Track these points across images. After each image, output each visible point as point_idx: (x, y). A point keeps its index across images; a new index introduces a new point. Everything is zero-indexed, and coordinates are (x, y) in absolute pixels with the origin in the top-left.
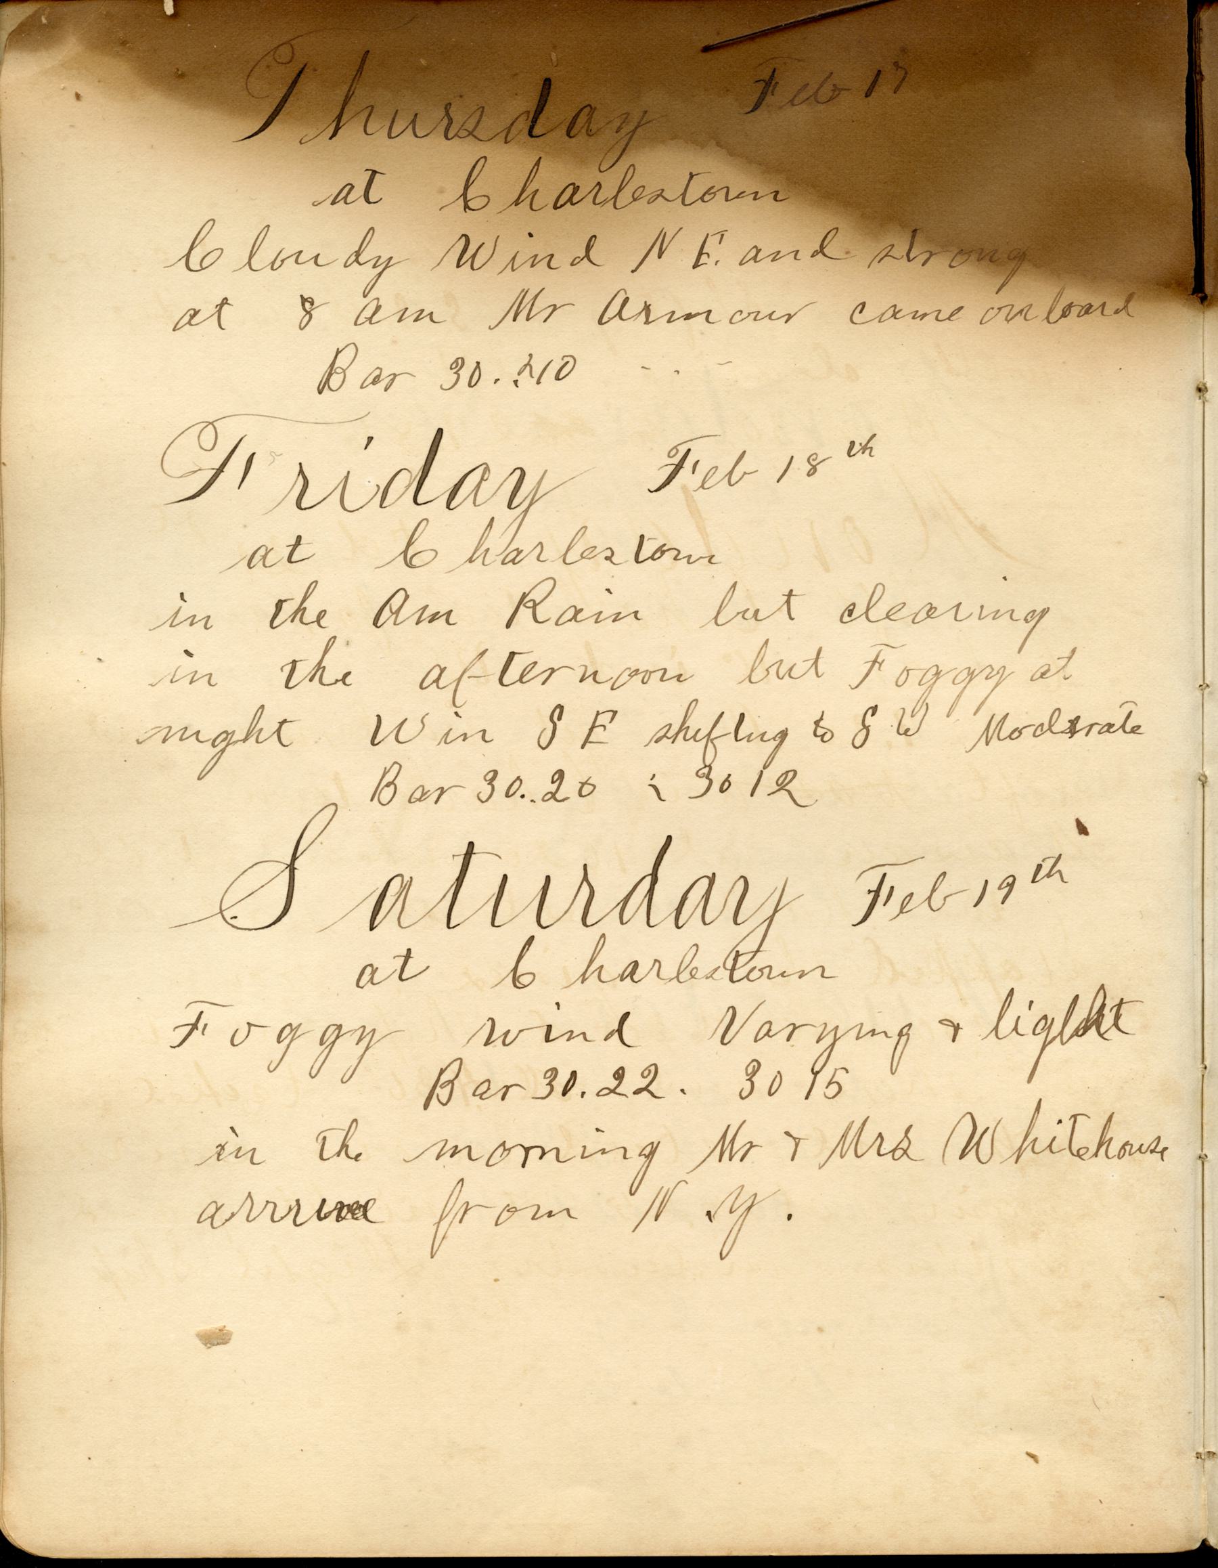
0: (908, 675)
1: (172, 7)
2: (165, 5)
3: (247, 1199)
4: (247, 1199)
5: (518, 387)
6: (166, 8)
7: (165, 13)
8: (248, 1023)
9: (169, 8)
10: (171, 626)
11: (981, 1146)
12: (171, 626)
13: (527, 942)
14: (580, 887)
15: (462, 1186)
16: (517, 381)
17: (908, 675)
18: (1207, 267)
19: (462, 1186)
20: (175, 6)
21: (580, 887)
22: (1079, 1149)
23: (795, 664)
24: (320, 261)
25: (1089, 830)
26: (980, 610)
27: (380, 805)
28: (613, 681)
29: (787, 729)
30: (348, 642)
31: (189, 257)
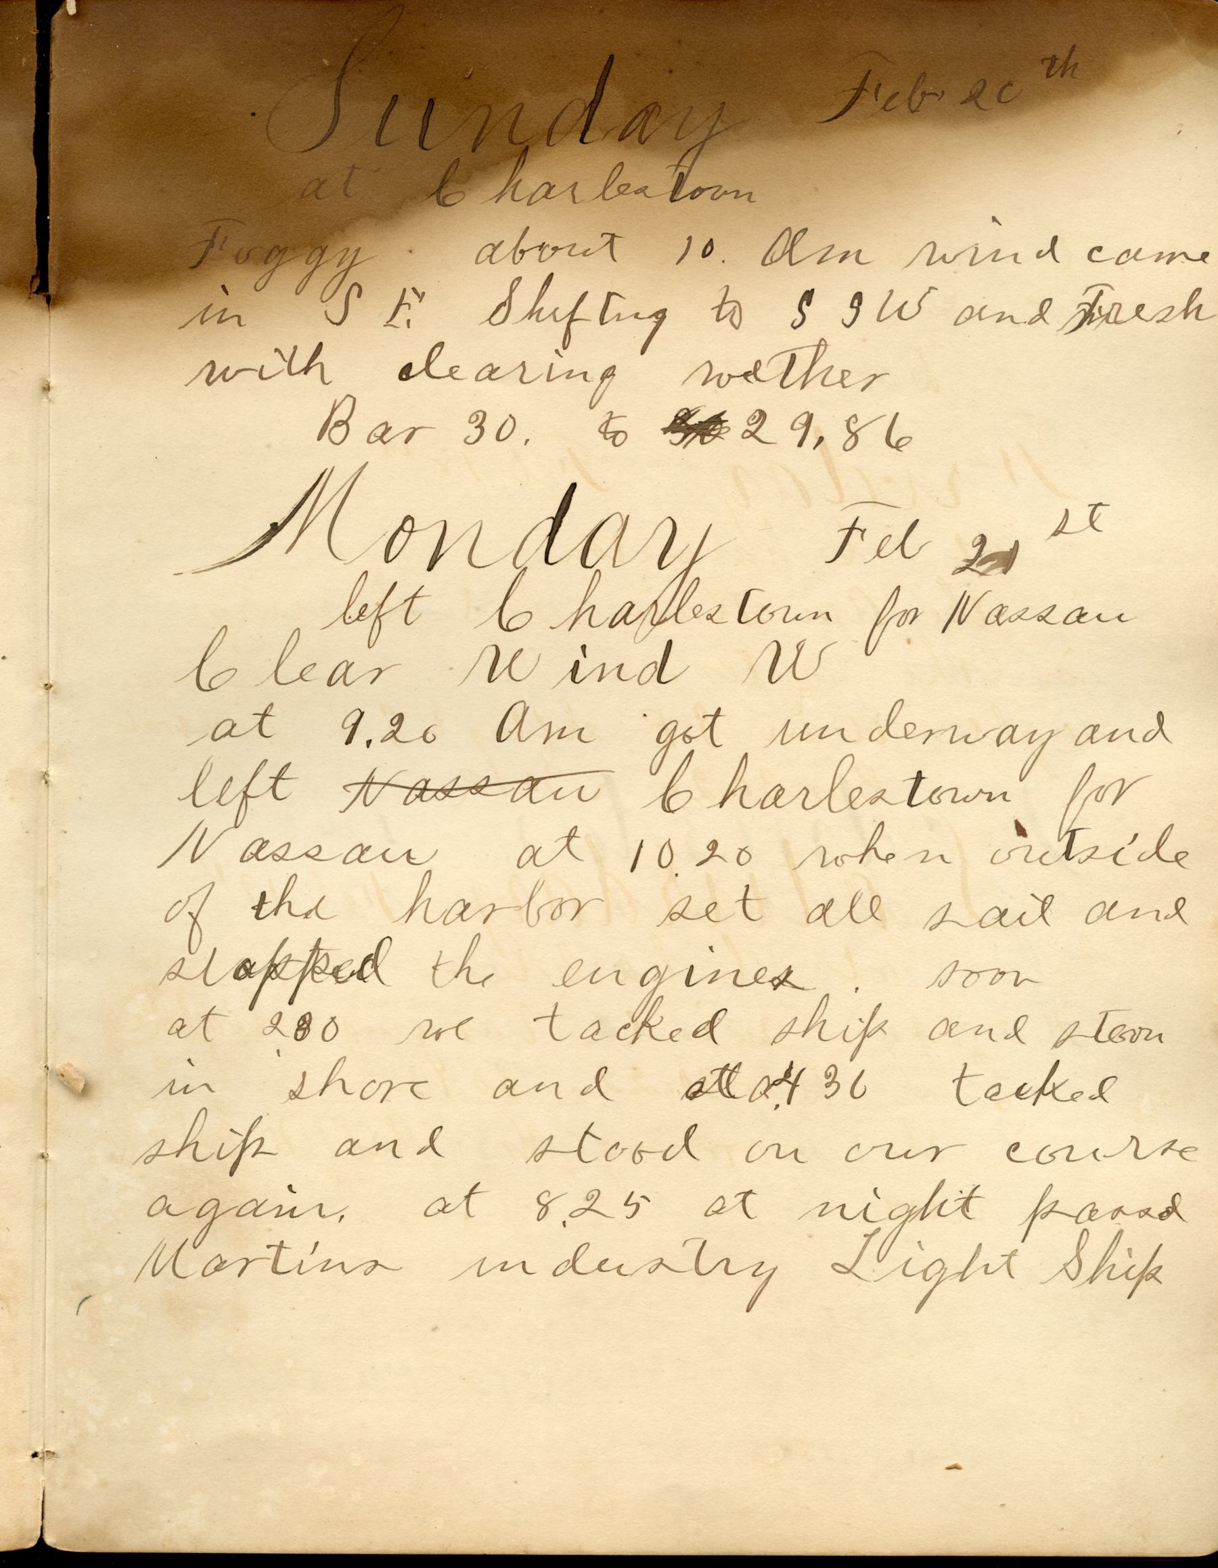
0: (380, 621)
1: (75, 7)
2: (67, 5)
3: (550, 316)
4: (550, 316)
5: (713, 952)
6: (68, 9)
7: (67, 12)
8: (865, 530)
9: (71, 7)
10: (820, 737)
11: (715, 729)
12: (820, 737)
13: (546, 282)
14: (563, 849)
15: (587, 1249)
16: (712, 947)
17: (380, 621)
18: (51, 267)
19: (587, 1249)
20: (78, 6)
21: (563, 849)
22: (672, 1032)
23: (642, 841)
24: (623, 1270)
25: (1027, 832)
26: (538, 1020)
27: (336, 446)
28: (238, 1209)
29: (662, 429)
30: (436, 1328)
31: (901, 312)
